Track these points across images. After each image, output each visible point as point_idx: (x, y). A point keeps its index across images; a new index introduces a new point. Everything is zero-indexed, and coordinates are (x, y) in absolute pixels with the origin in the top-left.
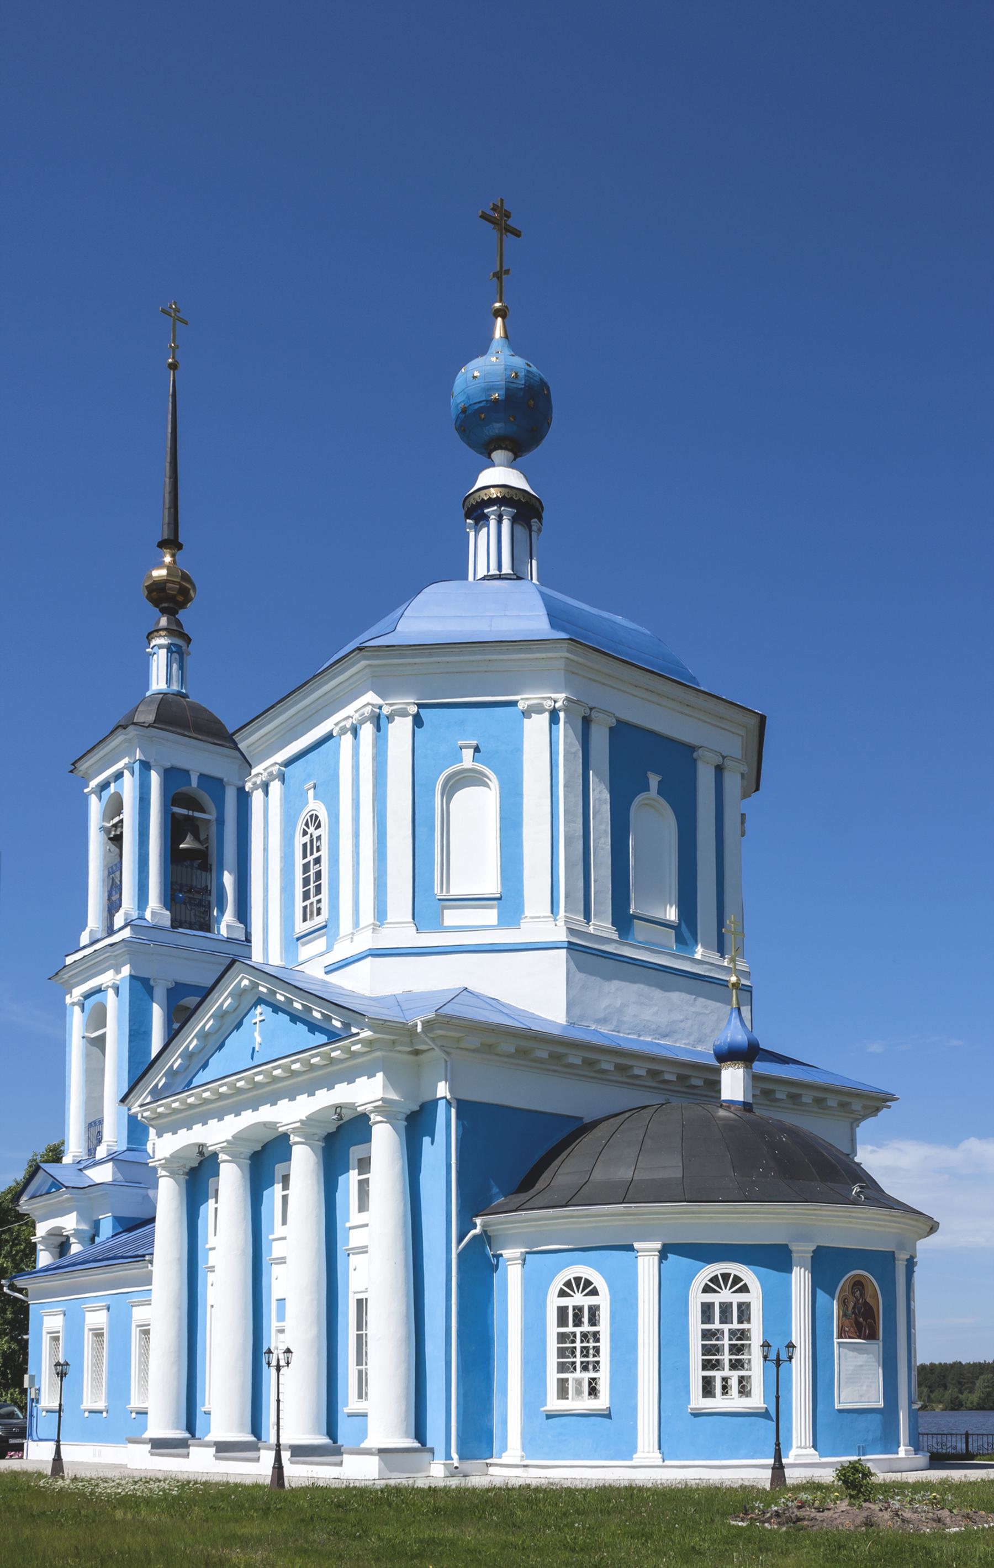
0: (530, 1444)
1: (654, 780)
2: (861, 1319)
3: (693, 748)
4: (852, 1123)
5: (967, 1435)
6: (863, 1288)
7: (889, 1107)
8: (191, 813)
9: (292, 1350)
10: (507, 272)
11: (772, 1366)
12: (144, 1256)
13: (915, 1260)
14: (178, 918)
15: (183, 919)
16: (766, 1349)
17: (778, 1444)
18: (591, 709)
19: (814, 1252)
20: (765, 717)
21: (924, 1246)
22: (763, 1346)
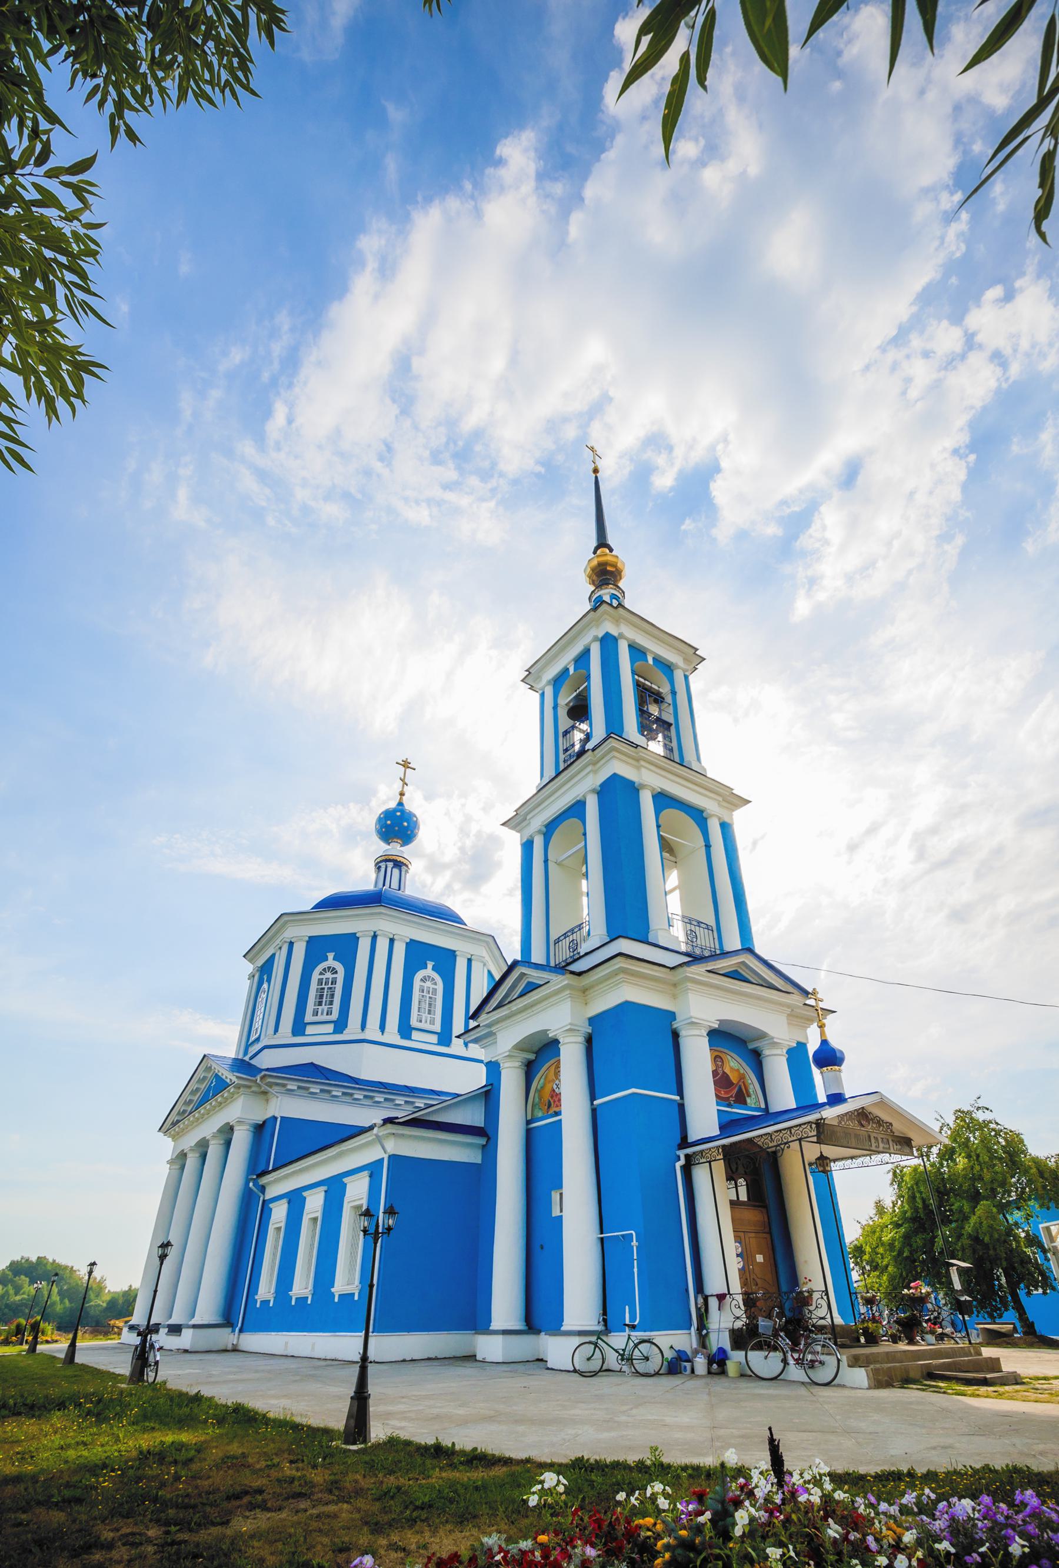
3: (455, 951)
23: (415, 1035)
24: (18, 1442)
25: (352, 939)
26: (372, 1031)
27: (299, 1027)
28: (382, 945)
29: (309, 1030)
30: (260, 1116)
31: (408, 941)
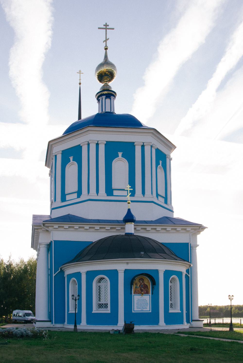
0: (89, 322)
2: (143, 289)
3: (134, 143)
5: (241, 320)
6: (144, 280)
23: (115, 193)
26: (148, 196)
27: (63, 199)
29: (68, 198)
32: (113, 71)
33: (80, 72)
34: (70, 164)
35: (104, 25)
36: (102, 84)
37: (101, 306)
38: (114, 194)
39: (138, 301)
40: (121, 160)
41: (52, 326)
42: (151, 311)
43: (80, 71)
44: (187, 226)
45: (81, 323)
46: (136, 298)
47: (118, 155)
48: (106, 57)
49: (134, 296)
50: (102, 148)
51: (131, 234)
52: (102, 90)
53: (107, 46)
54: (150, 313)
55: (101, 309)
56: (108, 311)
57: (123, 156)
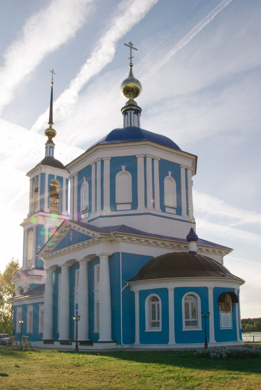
0: (178, 340)
1: (170, 173)
2: (226, 306)
4: (222, 256)
5: (254, 336)
7: (231, 252)
8: (54, 185)
9: (80, 316)
10: (133, 57)
11: (204, 318)
12: (42, 293)
13: (239, 291)
14: (51, 210)
15: (52, 210)
16: (202, 314)
17: (206, 339)
18: (154, 157)
19: (214, 289)
20: (197, 157)
21: (241, 287)
22: (201, 313)
23: (119, 207)
24: (213, 376)
25: (134, 159)
28: (149, 161)
30: (111, 252)
31: (160, 160)
32: (139, 89)
33: (52, 72)
34: (121, 172)
35: (129, 43)
36: (127, 99)
37: (154, 324)
38: (118, 209)
39: (224, 318)
40: (170, 179)
41: (119, 347)
42: (221, 329)
43: (53, 70)
44: (223, 249)
45: (169, 342)
46: (223, 315)
47: (122, 169)
48: (131, 73)
49: (221, 313)
50: (156, 164)
51: (194, 253)
52: (127, 105)
53: (132, 63)
54: (158, 332)
55: (190, 327)
56: (159, 329)
57: (172, 175)
